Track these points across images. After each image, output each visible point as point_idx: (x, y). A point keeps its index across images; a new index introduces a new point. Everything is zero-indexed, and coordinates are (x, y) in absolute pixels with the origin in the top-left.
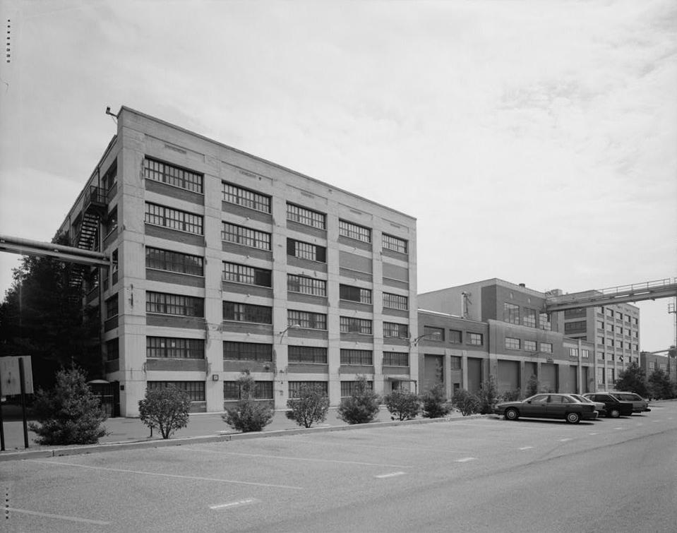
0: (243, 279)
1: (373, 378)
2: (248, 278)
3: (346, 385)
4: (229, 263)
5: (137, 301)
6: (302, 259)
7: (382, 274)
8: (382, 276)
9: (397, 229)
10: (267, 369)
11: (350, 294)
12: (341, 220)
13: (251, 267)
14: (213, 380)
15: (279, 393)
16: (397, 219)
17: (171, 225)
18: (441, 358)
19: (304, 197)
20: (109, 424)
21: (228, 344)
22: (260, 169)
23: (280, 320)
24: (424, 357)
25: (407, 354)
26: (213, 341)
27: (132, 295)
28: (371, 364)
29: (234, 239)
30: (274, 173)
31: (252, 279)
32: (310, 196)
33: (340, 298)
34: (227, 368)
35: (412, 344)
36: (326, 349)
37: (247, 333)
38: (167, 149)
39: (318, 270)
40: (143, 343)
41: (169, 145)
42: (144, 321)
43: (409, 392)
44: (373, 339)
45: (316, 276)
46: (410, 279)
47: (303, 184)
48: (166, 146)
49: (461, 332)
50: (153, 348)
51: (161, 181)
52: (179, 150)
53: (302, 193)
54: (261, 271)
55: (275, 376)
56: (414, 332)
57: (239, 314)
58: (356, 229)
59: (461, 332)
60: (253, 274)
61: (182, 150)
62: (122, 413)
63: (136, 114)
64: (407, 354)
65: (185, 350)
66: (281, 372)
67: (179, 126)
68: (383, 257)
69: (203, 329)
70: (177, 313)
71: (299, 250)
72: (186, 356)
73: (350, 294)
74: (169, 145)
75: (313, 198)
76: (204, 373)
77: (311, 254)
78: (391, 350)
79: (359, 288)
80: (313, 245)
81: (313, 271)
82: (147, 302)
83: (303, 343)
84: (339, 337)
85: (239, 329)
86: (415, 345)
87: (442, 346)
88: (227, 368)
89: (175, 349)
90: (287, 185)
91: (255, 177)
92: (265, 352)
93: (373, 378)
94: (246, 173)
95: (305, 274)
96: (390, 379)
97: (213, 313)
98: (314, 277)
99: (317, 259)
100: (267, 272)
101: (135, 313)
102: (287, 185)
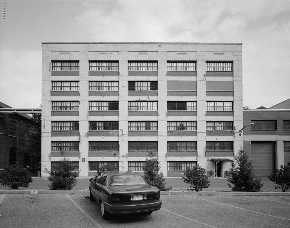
0: (102, 109)
1: (197, 159)
2: (105, 107)
3: (93, 165)
4: (210, 101)
5: (47, 126)
6: (140, 91)
7: (166, 90)
8: (205, 91)
9: (222, 55)
10: (115, 155)
11: (175, 106)
12: (207, 62)
13: (106, 101)
14: (83, 161)
15: (122, 168)
16: (220, 48)
17: (64, 89)
18: (274, 144)
19: (140, 55)
20: (34, 178)
21: (209, 143)
22: (111, 48)
23: (123, 126)
24: (250, 143)
25: (232, 142)
26: (82, 142)
27: (45, 124)
28: (196, 150)
29: (96, 87)
30: (119, 47)
31: (107, 108)
32: (145, 54)
33: (167, 110)
34: (90, 155)
35: (237, 135)
36: (157, 142)
37: (102, 136)
38: (62, 55)
39: (150, 96)
40: (50, 144)
41: (62, 52)
42: (50, 134)
43: (283, 171)
44: (197, 133)
45: (149, 99)
46: (197, 90)
47: (140, 47)
48: (61, 53)
49: (276, 121)
50: (55, 147)
51: (60, 70)
52: (66, 53)
53: (139, 53)
54: (113, 103)
55: (119, 159)
56: (239, 125)
57: (99, 127)
58: (221, 65)
59: (276, 121)
60: (108, 105)
61: (68, 52)
62: (221, 175)
63: (47, 44)
64: (232, 142)
65: (70, 147)
66: (123, 156)
67: (53, 42)
68: (206, 77)
69: (78, 136)
70: (134, 130)
71: (138, 86)
72: (70, 150)
73: (175, 106)
74: (62, 52)
75: (147, 54)
76: (78, 157)
77: (147, 87)
78: (215, 140)
79: (186, 102)
80: (148, 82)
81: (147, 97)
82: (206, 126)
83: (217, 139)
84: (166, 134)
85: (99, 134)
86: (240, 135)
87: (275, 134)
88: (90, 155)
89: (66, 146)
90: (52, 51)
91: (108, 53)
92: (115, 145)
93: (197, 159)
94: (103, 52)
95: (141, 99)
96: (212, 161)
97: (84, 127)
98: (148, 100)
99: (151, 90)
100: (116, 103)
101: (46, 132)
102: (52, 51)
